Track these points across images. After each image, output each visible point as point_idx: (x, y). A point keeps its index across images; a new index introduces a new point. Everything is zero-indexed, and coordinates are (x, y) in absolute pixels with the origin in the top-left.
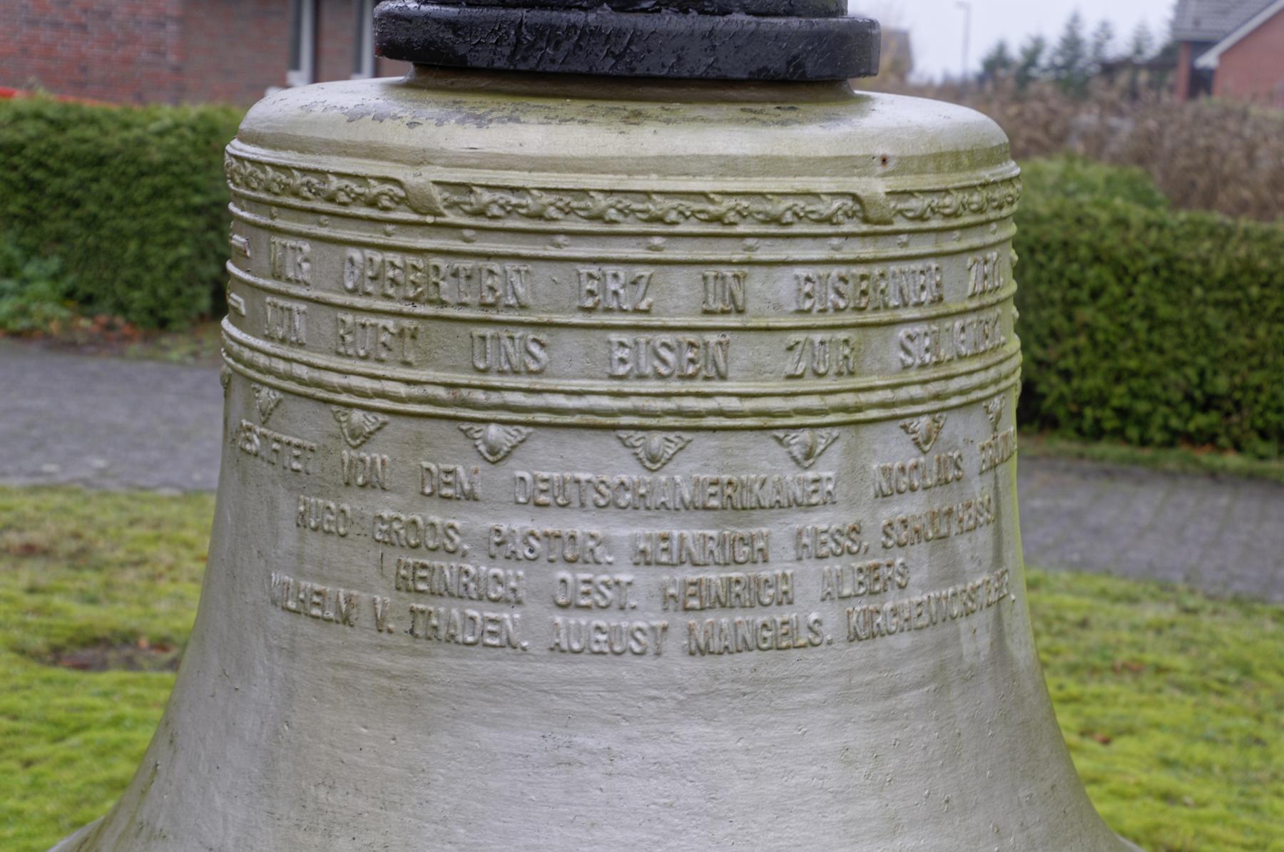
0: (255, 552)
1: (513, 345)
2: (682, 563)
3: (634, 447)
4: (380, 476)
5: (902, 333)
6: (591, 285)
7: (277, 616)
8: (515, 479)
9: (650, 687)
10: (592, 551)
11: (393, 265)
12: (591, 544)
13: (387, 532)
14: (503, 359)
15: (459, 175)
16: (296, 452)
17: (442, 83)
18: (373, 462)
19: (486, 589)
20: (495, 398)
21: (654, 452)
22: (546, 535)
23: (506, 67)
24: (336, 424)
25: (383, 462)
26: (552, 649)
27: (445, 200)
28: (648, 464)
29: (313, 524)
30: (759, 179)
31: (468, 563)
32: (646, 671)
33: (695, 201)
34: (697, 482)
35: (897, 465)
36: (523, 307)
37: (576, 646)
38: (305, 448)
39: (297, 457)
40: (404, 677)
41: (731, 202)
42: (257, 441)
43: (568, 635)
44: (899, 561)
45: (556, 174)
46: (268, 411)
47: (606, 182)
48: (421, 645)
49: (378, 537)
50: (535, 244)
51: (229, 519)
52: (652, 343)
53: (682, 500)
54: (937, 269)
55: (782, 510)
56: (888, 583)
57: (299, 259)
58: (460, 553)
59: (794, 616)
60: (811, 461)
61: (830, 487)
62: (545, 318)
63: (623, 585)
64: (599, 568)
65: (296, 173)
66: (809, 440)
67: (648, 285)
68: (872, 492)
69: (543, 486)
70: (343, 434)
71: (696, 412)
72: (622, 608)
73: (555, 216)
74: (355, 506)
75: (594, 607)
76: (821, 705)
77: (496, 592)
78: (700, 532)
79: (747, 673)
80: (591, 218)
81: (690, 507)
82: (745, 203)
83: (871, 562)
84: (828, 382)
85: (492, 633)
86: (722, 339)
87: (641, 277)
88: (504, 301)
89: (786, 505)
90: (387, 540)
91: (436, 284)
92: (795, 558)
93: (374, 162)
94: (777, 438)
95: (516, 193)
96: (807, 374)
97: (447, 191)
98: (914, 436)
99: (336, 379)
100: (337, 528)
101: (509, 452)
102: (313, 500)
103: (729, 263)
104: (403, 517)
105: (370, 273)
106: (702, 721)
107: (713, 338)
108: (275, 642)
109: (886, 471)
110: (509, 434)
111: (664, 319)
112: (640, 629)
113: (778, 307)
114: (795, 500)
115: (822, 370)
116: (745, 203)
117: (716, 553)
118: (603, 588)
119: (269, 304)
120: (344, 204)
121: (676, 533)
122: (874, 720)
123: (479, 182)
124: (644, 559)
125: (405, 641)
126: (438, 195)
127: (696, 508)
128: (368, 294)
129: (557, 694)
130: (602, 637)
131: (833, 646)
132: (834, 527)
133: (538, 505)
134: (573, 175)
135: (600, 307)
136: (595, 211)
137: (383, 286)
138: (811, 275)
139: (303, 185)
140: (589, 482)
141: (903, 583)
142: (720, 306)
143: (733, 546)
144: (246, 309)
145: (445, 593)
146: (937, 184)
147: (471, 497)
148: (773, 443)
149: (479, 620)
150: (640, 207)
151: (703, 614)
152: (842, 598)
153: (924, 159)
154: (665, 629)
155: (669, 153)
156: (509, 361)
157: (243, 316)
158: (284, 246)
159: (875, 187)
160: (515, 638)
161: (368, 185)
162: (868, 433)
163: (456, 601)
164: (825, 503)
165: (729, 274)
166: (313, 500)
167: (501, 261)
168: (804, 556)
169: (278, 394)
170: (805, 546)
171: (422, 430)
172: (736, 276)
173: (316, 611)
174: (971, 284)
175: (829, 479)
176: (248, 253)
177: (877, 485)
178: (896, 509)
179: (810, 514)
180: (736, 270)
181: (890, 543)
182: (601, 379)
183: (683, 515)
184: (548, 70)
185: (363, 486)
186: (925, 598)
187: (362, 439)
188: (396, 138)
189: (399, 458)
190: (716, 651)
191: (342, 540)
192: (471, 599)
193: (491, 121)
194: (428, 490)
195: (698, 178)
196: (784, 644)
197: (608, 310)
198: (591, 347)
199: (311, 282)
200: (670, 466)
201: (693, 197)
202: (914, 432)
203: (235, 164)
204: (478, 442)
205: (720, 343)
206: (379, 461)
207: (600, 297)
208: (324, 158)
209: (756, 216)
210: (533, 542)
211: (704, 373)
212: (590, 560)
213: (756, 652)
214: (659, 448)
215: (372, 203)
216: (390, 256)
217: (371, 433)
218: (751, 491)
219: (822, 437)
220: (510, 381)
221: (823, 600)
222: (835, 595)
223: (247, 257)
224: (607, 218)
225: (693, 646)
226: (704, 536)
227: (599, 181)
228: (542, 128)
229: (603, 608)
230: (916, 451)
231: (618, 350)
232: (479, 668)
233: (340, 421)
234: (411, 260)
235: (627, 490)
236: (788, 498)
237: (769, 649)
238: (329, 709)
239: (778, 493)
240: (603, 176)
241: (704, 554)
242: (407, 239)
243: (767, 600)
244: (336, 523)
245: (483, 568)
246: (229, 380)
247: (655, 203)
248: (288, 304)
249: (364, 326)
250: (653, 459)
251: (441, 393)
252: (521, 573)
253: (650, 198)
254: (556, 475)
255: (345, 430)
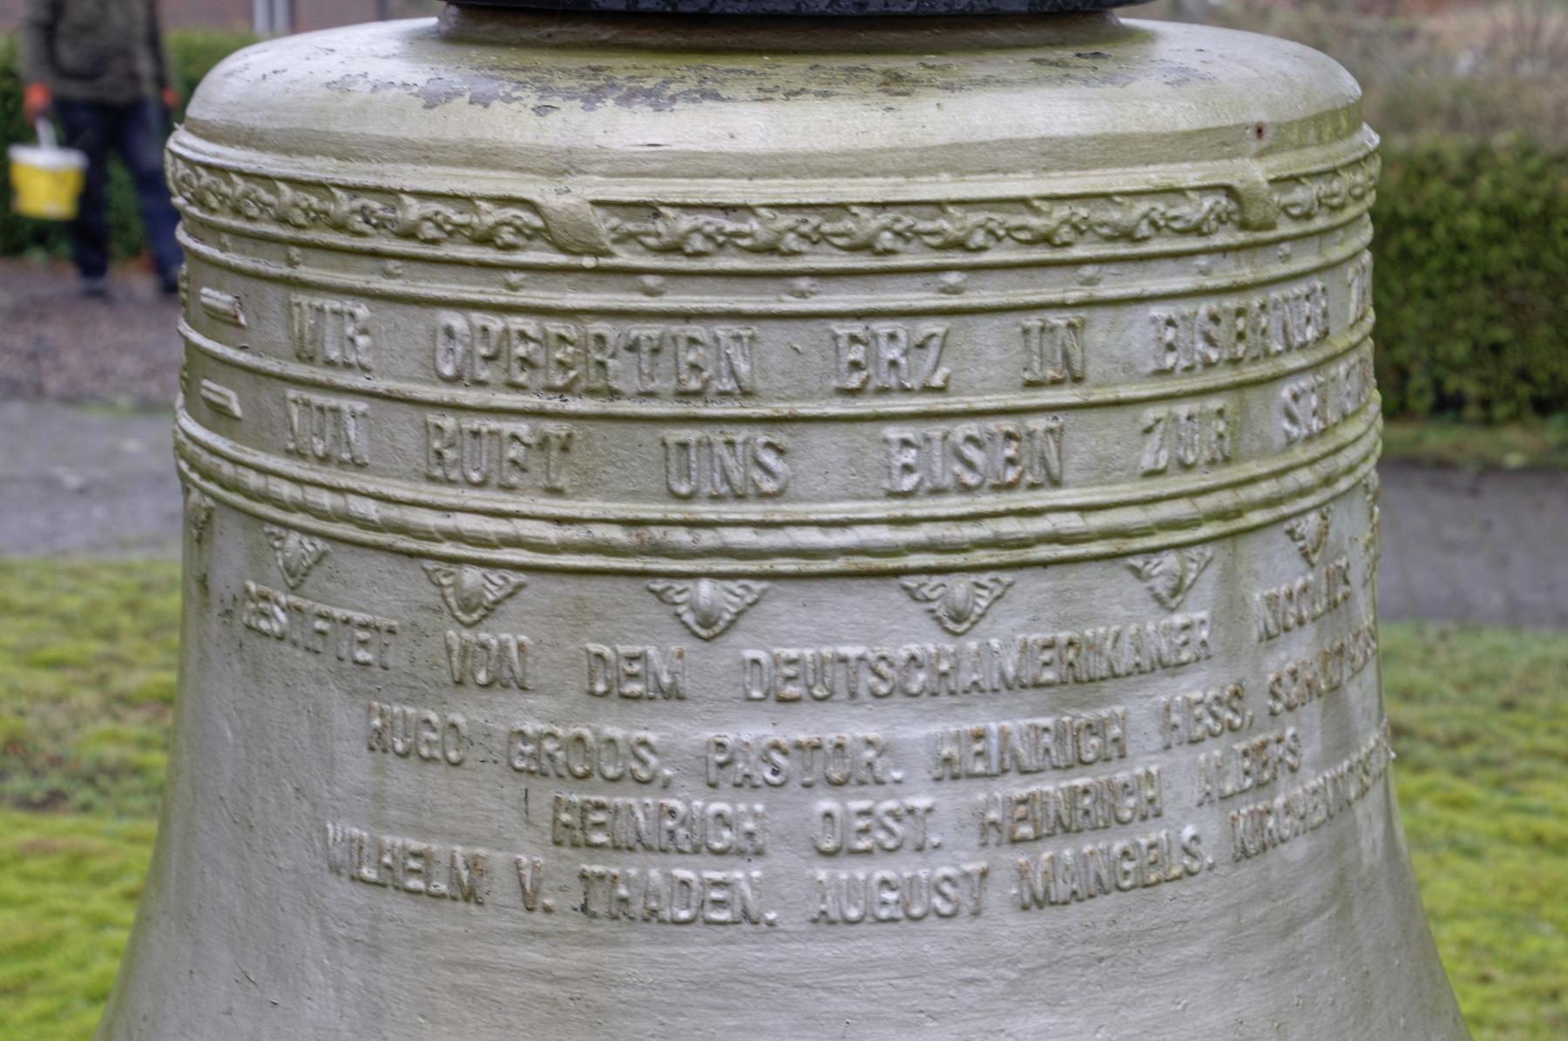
0: (290, 789)
1: (734, 455)
2: (1005, 771)
3: (928, 600)
4: (518, 669)
5: (1285, 393)
6: (857, 353)
7: (342, 888)
8: (743, 662)
9: (966, 964)
10: (870, 765)
11: (523, 336)
12: (870, 754)
13: (532, 756)
14: (717, 477)
15: (634, 189)
16: (362, 635)
17: (530, 34)
18: (503, 647)
19: (704, 835)
20: (707, 538)
21: (960, 606)
22: (799, 746)
23: (659, 8)
24: (433, 589)
25: (521, 647)
26: (815, 921)
27: (614, 230)
28: (951, 625)
29: (400, 747)
30: (1098, 172)
31: (673, 797)
32: (959, 940)
33: (1009, 212)
34: (1025, 648)
35: (1284, 589)
36: (747, 394)
37: (853, 913)
38: (377, 629)
39: (363, 643)
40: (575, 980)
41: (1062, 211)
42: (282, 616)
43: (837, 898)
44: (1290, 732)
45: (793, 181)
46: (302, 570)
47: (875, 190)
48: (602, 928)
49: (519, 764)
50: (762, 293)
51: (229, 734)
52: (951, 438)
53: (1003, 676)
54: (1324, 290)
55: (1142, 677)
56: (1279, 767)
57: (350, 330)
58: (659, 783)
59: (1163, 834)
60: (1179, 598)
61: (1204, 634)
62: (784, 409)
63: (919, 813)
64: (881, 790)
65: (338, 193)
66: (1177, 567)
67: (943, 346)
68: (1255, 634)
69: (789, 671)
70: (448, 605)
71: (1020, 539)
72: (920, 849)
73: (796, 249)
74: (474, 717)
75: (877, 851)
76: (1203, 963)
77: (720, 838)
78: (1029, 721)
79: (1103, 929)
80: (853, 249)
81: (1016, 685)
82: (1083, 212)
83: (1257, 740)
84: (1197, 477)
85: (718, 903)
86: (1053, 425)
87: (932, 336)
88: (717, 385)
89: (1148, 668)
90: (533, 768)
91: (601, 364)
92: (1160, 747)
93: (481, 173)
94: (1133, 569)
95: (732, 214)
96: (1170, 467)
97: (616, 215)
98: (1301, 544)
99: (431, 520)
100: (444, 753)
101: (732, 623)
102: (396, 709)
103: (1062, 306)
104: (560, 731)
105: (484, 351)
106: (1045, 1007)
107: (1039, 424)
108: (341, 932)
109: (1271, 601)
110: (732, 593)
111: (967, 399)
112: (947, 879)
113: (1129, 370)
114: (1160, 660)
115: (1191, 458)
116: (1083, 212)
117: (1053, 753)
118: (889, 822)
119: (295, 401)
120: (433, 242)
121: (994, 727)
122: (1270, 973)
123: (671, 200)
124: (949, 771)
125: (574, 924)
126: (605, 224)
127: (1023, 686)
128: (481, 384)
129: (824, 989)
130: (890, 896)
131: (1216, 871)
132: (1211, 694)
133: (782, 700)
134: (820, 181)
135: (871, 386)
136: (861, 237)
137: (507, 370)
138: (1173, 316)
139: (353, 212)
140: (861, 659)
141: (1296, 764)
142: (1050, 373)
143: (1076, 739)
144: (242, 407)
145: (638, 846)
146: (1323, 161)
147: (673, 694)
148: (1128, 576)
149: (695, 885)
150: (929, 226)
151: (1039, 845)
152: (1224, 798)
153: (1304, 123)
154: (984, 874)
155: (965, 138)
156: (727, 479)
157: (237, 419)
158: (320, 310)
159: (1254, 172)
160: (754, 909)
161: (476, 211)
162: (1248, 546)
163: (654, 858)
164: (1198, 659)
165: (1062, 323)
166: (396, 709)
167: (707, 322)
168: (1174, 743)
169: (319, 543)
170: (1175, 727)
171: (586, 594)
172: (1071, 326)
173: (414, 883)
174: (1353, 307)
175: (1203, 622)
176: (242, 320)
177: (1262, 624)
178: (1283, 655)
179: (1179, 678)
180: (1070, 316)
181: (1279, 707)
182: (874, 498)
183: (1005, 698)
184: (729, 10)
185: (486, 686)
186: (1321, 780)
187: (481, 612)
188: (517, 133)
189: (548, 640)
190: (1060, 900)
191: (453, 770)
192: (681, 852)
193: (673, 99)
194: (600, 687)
195: (1011, 175)
196: (1153, 878)
197: (883, 391)
198: (857, 450)
199: (373, 366)
200: (983, 625)
201: (1007, 206)
202: (1302, 538)
203: (183, 170)
204: (681, 609)
205: (1051, 431)
206: (513, 645)
207: (871, 370)
208: (388, 168)
209: (1097, 228)
210: (777, 757)
211: (1029, 478)
212: (869, 779)
213: (1115, 894)
214: (967, 601)
215: (485, 239)
216: (517, 323)
217: (497, 602)
218: (1100, 653)
219: (1193, 561)
220: (730, 511)
221: (1200, 804)
222: (1215, 795)
223: (239, 326)
224: (879, 247)
225: (1027, 897)
226: (1036, 728)
227: (864, 189)
228: (761, 108)
229: (890, 851)
230: (1303, 566)
231: (900, 452)
232: (699, 958)
233: (440, 585)
234: (554, 327)
235: (920, 667)
236: (1151, 658)
237: (1133, 887)
238: (449, 1033)
239: (1138, 651)
240: (867, 180)
241: (1037, 753)
242: (547, 294)
243: (1127, 814)
244: (443, 745)
245: (698, 804)
246: (209, 517)
247: (951, 219)
248: (331, 401)
249: (476, 434)
250: (959, 617)
251: (617, 534)
252: (759, 807)
253: (944, 212)
254: (808, 653)
255: (452, 600)
